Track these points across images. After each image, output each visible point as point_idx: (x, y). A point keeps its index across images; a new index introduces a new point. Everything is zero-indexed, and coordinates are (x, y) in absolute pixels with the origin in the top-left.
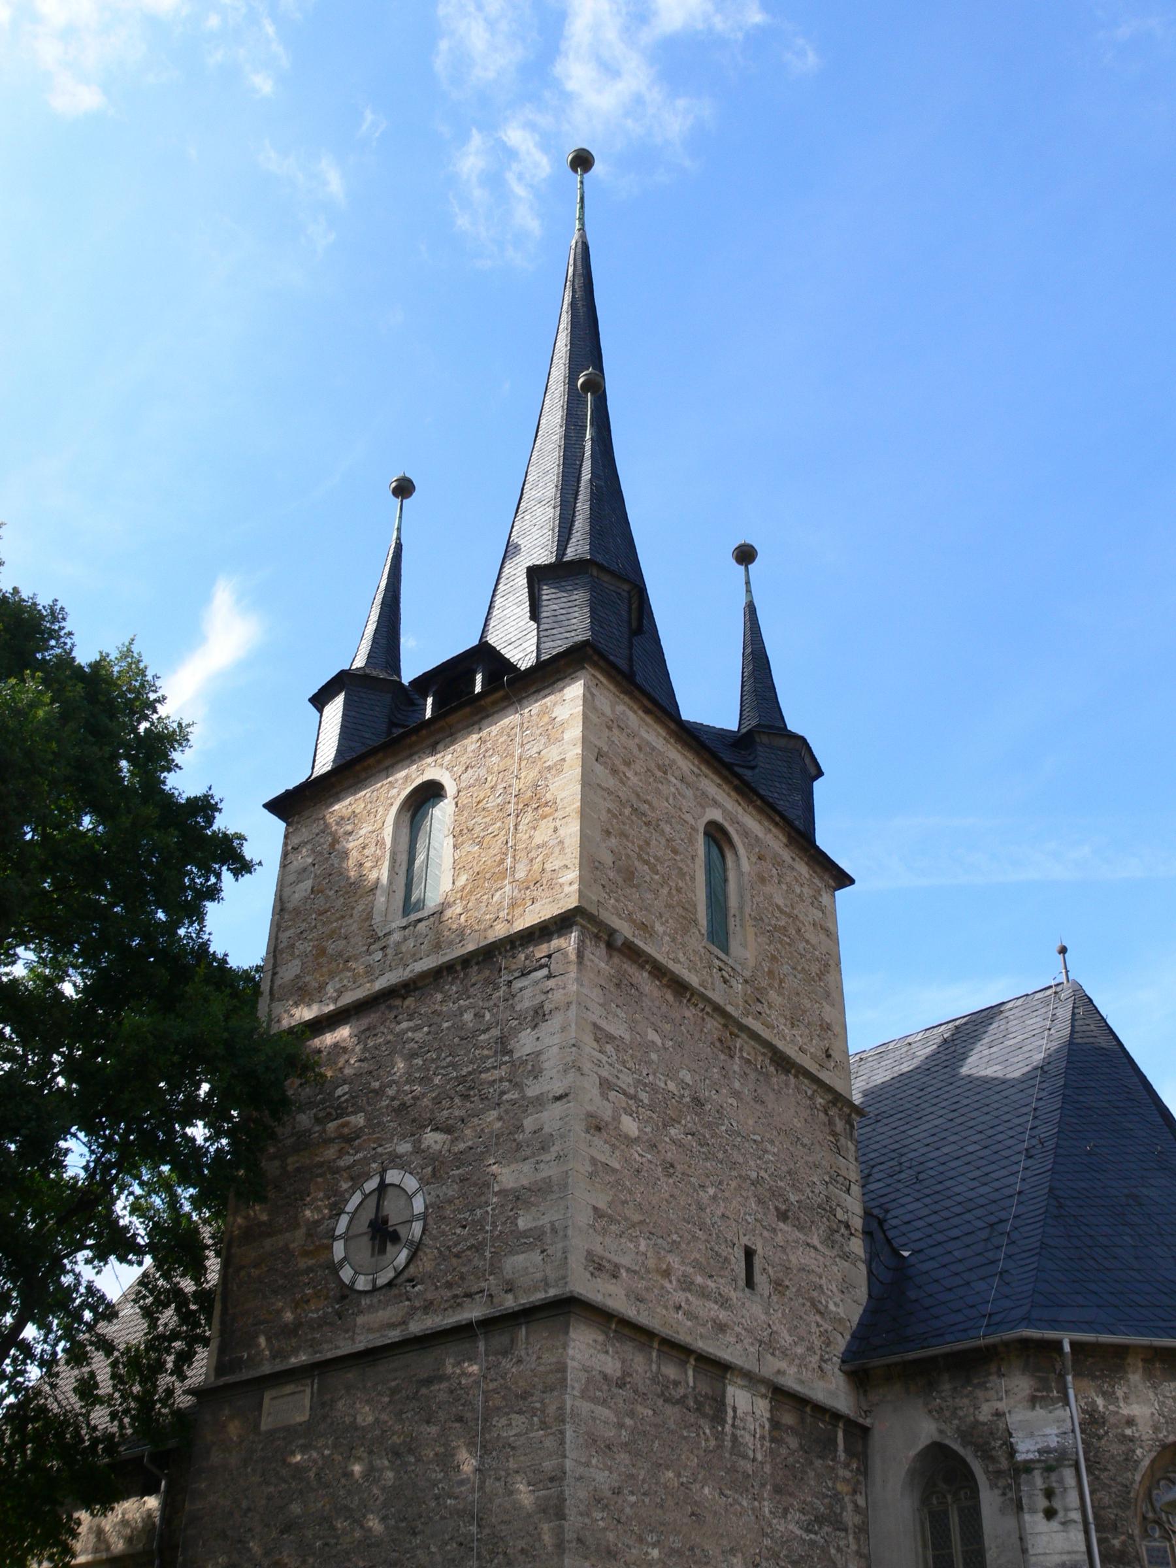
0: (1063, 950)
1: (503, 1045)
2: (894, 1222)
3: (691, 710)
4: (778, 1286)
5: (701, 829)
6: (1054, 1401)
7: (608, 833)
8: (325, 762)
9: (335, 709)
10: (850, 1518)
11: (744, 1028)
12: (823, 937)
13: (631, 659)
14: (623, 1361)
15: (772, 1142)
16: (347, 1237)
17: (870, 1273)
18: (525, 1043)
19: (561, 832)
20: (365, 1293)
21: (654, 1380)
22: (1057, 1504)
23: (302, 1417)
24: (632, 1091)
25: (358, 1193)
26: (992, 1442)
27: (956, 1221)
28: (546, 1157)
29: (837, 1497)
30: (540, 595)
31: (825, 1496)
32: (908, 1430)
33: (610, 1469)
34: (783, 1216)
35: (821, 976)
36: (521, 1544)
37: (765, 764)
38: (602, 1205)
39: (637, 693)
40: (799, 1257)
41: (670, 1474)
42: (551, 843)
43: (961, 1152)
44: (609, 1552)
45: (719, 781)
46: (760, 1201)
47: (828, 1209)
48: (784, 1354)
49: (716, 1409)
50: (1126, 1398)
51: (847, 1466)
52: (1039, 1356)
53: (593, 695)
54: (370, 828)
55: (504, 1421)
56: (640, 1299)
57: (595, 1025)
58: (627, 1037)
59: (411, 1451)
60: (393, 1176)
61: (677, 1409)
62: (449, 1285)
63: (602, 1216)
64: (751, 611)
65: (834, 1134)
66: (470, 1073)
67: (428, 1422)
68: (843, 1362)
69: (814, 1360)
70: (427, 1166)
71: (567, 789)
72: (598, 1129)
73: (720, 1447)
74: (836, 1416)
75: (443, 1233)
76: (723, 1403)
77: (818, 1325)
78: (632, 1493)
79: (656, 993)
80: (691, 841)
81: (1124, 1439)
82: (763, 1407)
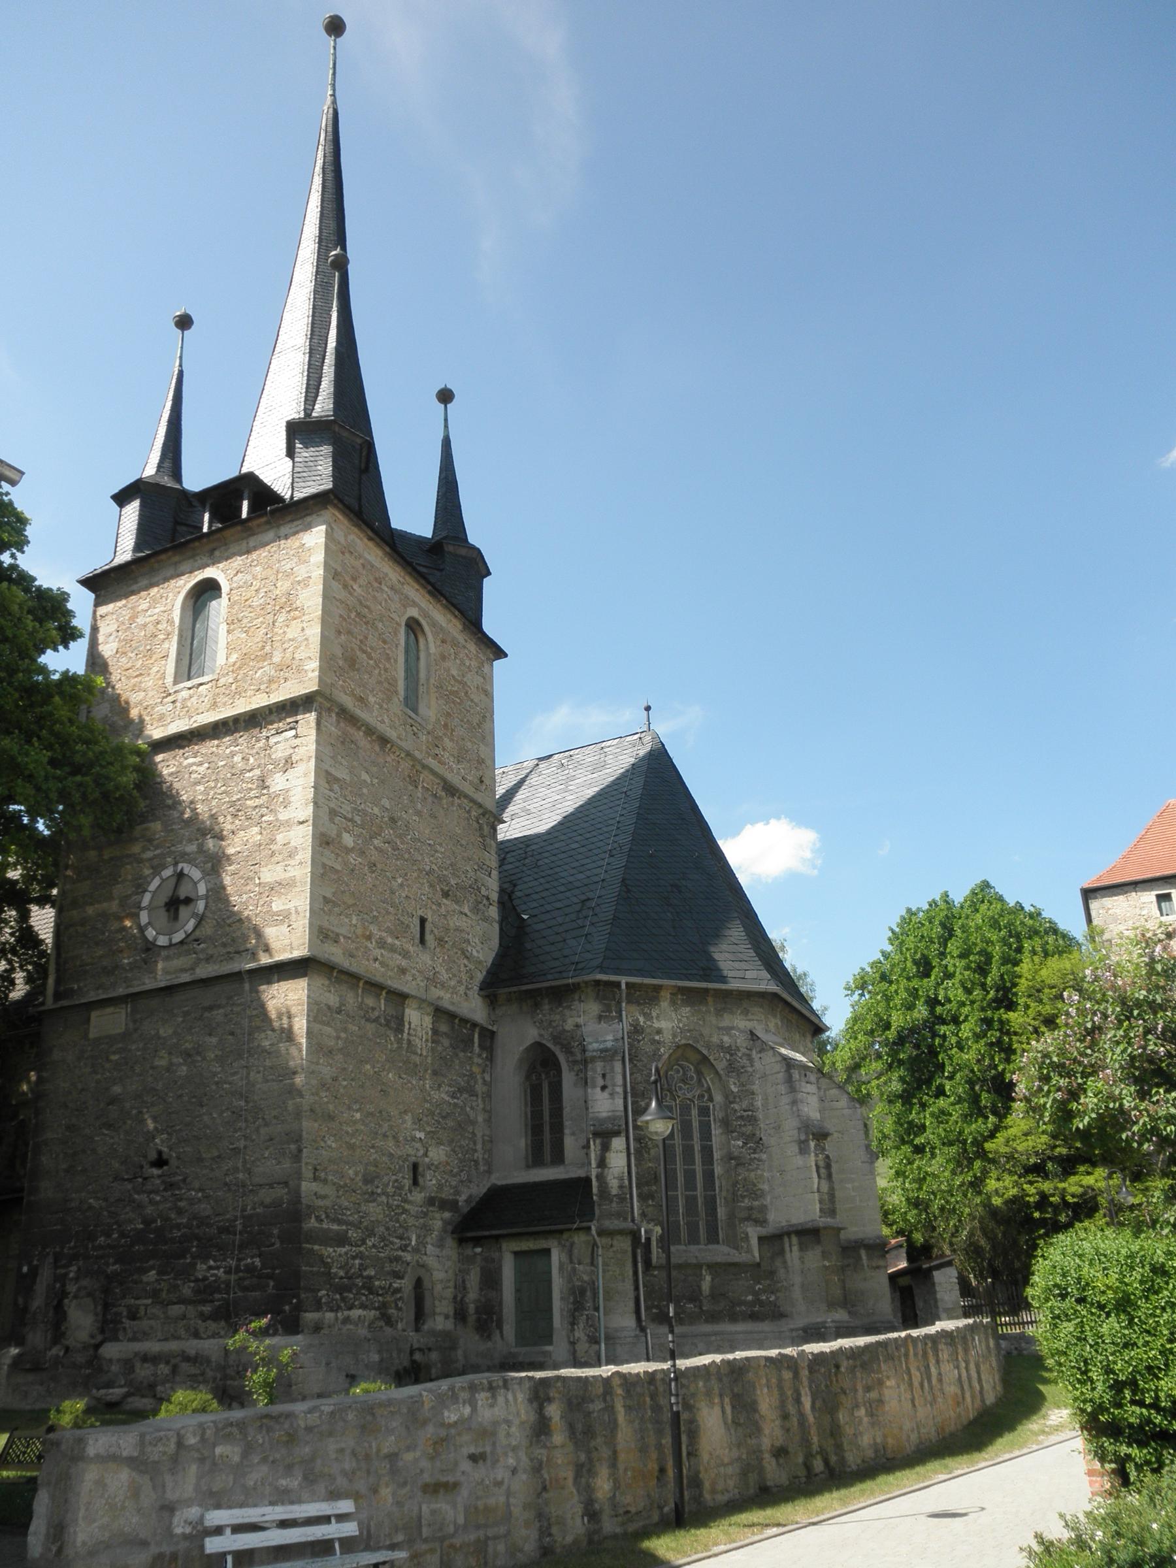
1: (263, 783)
2: (519, 894)
3: (398, 522)
4: (441, 941)
5: (403, 624)
6: (613, 1018)
7: (339, 632)
8: (125, 554)
9: (133, 509)
10: (480, 1088)
11: (424, 767)
12: (483, 696)
13: (360, 499)
14: (341, 996)
15: (440, 845)
16: (151, 908)
17: (501, 929)
18: (278, 782)
19: (307, 632)
20: (164, 947)
21: (360, 1008)
22: (608, 1083)
23: (120, 1029)
24: (350, 816)
25: (158, 878)
26: (571, 1042)
27: (560, 896)
28: (292, 862)
29: (472, 1076)
30: (294, 448)
31: (465, 1075)
32: (519, 1034)
33: (331, 1066)
34: (446, 895)
35: (479, 725)
36: (274, 1113)
37: (447, 567)
38: (329, 895)
39: (364, 527)
40: (455, 921)
41: (368, 1067)
42: (300, 639)
43: (567, 848)
44: (330, 1116)
46: (431, 886)
47: (475, 887)
48: (443, 986)
49: (397, 1023)
50: (658, 1017)
51: (480, 1056)
52: (606, 991)
53: (332, 529)
54: (163, 609)
55: (263, 1035)
56: (352, 956)
57: (327, 771)
58: (348, 778)
59: (199, 1053)
60: (187, 868)
61: (373, 1025)
62: (224, 945)
64: (447, 444)
65: (482, 836)
66: (239, 800)
67: (210, 1035)
68: (481, 989)
69: (462, 989)
70: (208, 862)
71: (312, 599)
72: (328, 843)
73: (400, 1048)
74: (475, 1025)
75: (220, 910)
76: (402, 1020)
77: (466, 966)
78: (344, 1080)
79: (368, 746)
80: (396, 632)
81: (654, 1042)
82: (428, 1021)
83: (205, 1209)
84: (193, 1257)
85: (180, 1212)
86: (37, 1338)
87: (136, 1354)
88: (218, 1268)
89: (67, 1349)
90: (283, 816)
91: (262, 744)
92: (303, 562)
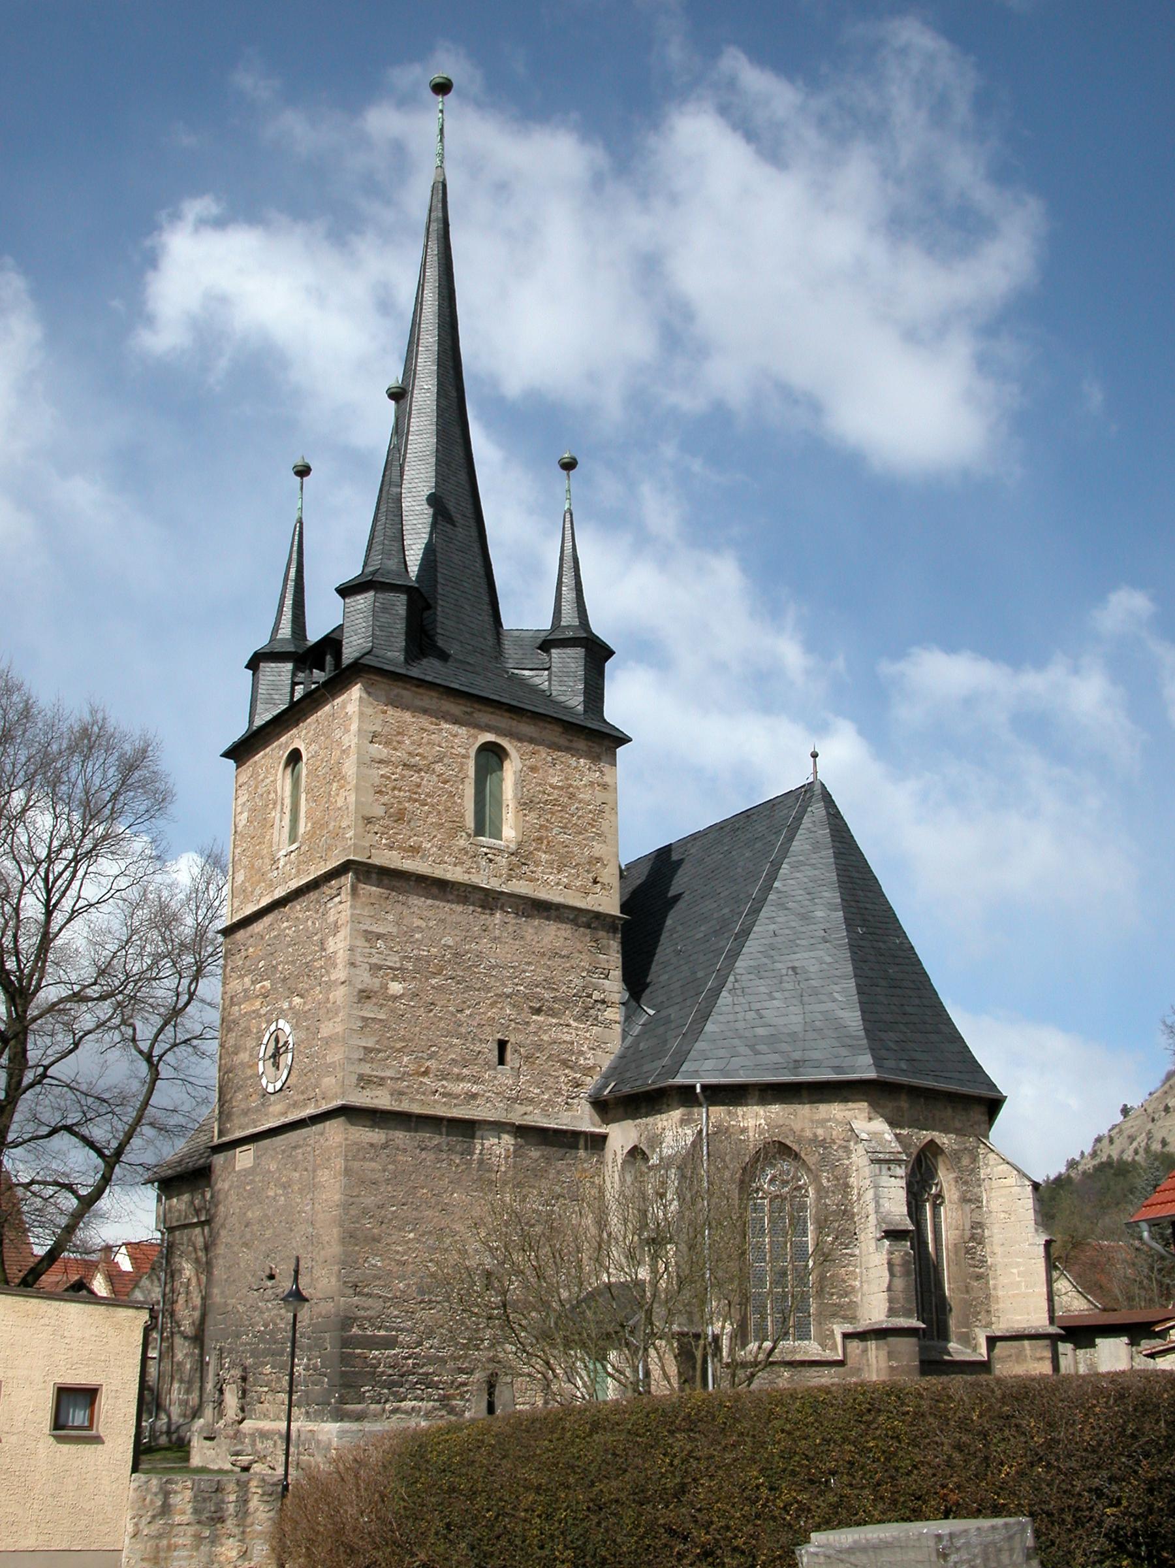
0: (815, 755)
24: (398, 965)
45: (491, 710)
63: (371, 1052)
77: (567, 1076)
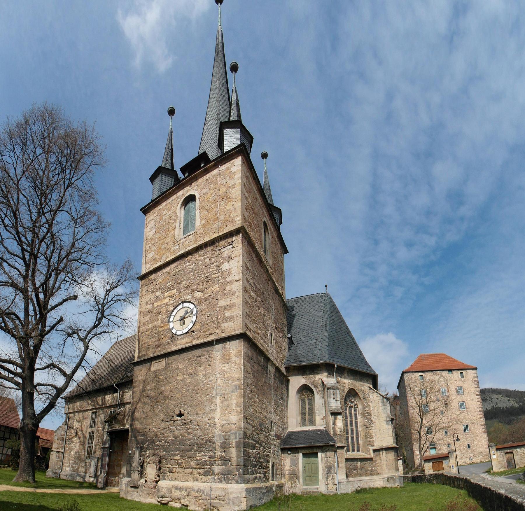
18: (225, 266)
19: (235, 206)
59: (195, 374)
83: (199, 433)
84: (195, 451)
85: (189, 434)
86: (135, 476)
87: (173, 486)
88: (206, 456)
89: (146, 481)
90: (229, 279)
91: (218, 252)
92: (231, 178)
